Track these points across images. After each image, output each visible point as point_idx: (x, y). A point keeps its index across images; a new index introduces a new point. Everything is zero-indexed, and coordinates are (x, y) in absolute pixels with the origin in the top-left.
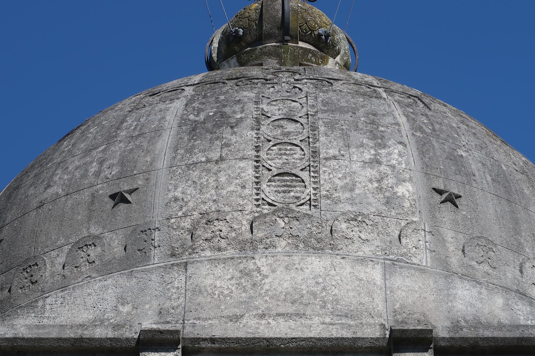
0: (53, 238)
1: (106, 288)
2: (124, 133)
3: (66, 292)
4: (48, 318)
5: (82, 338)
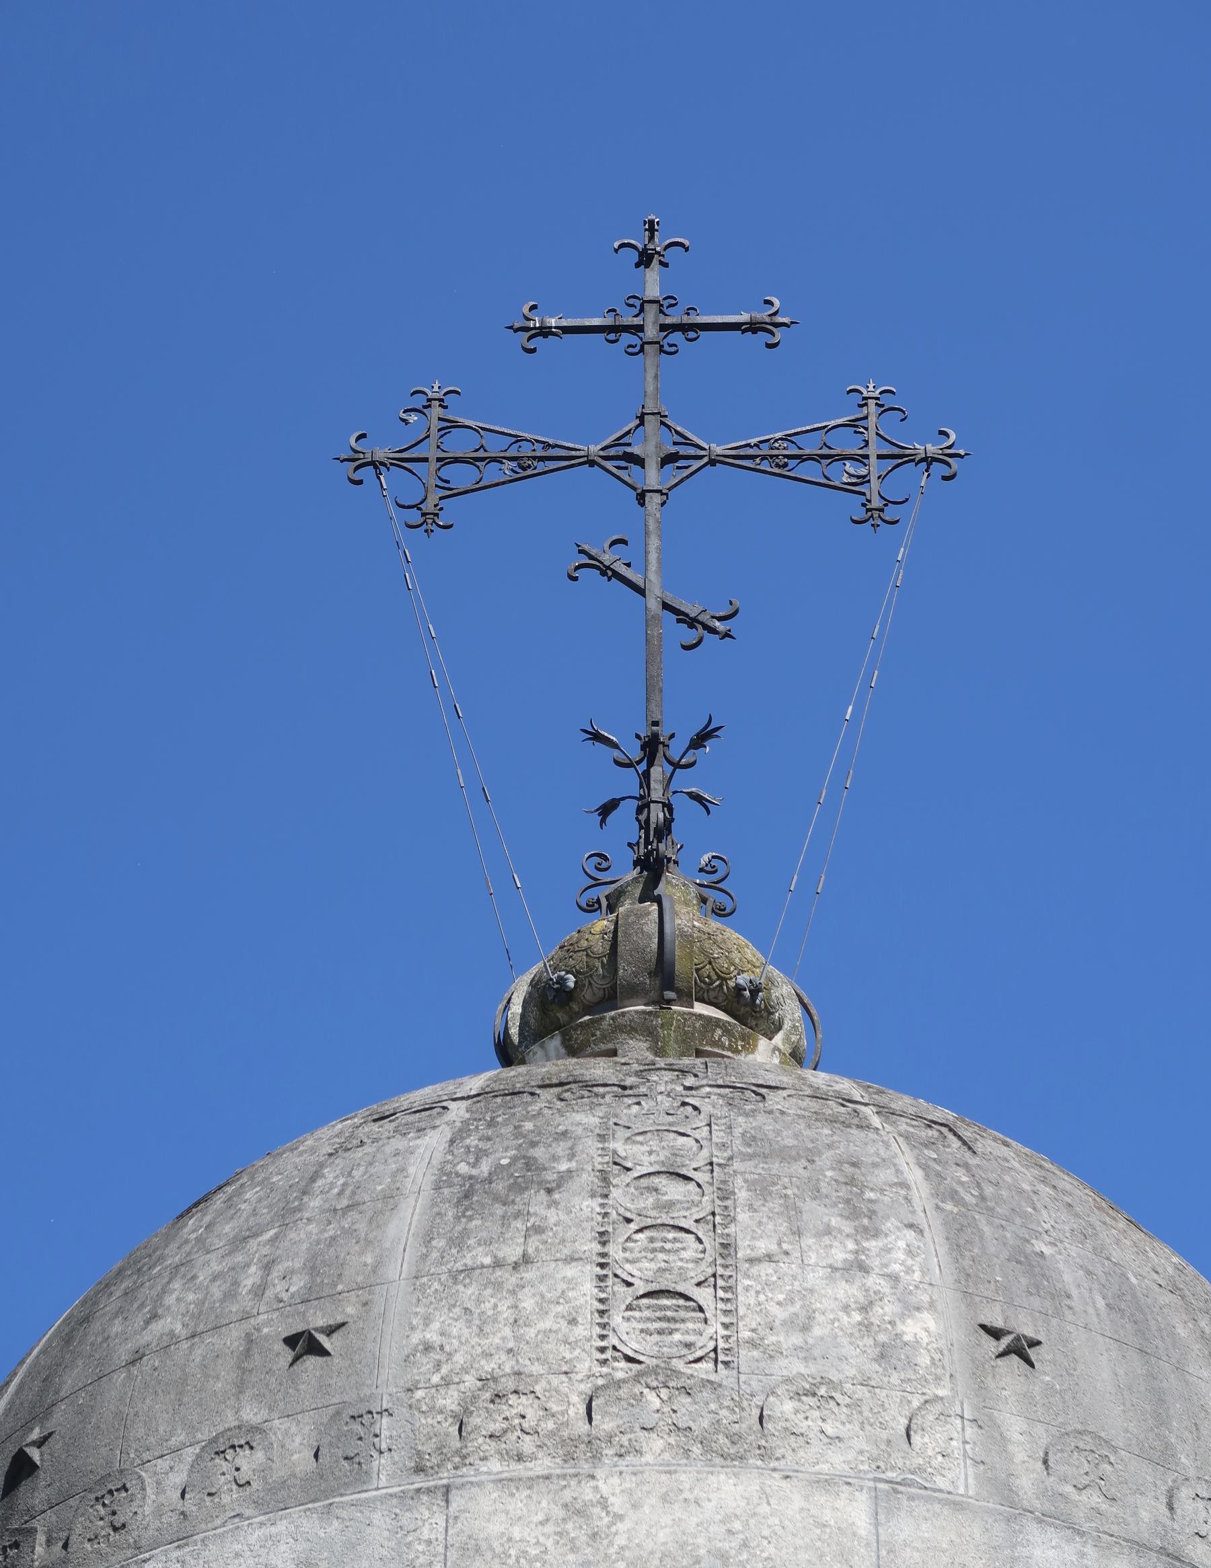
0: (161, 1429)
1: (275, 1540)
3: (187, 1549)
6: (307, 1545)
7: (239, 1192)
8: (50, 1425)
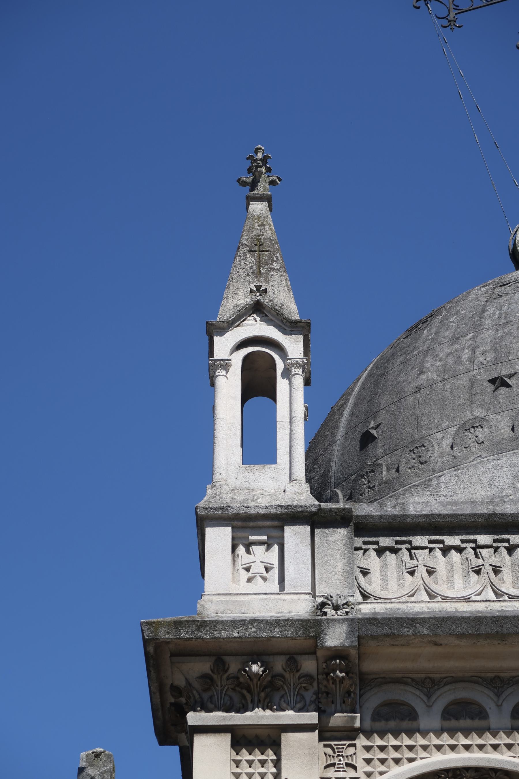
0: (436, 420)
1: (501, 466)
2: (489, 322)
3: (460, 471)
4: (445, 495)
5: (496, 514)
6: (516, 468)
7: (446, 317)
8: (379, 420)
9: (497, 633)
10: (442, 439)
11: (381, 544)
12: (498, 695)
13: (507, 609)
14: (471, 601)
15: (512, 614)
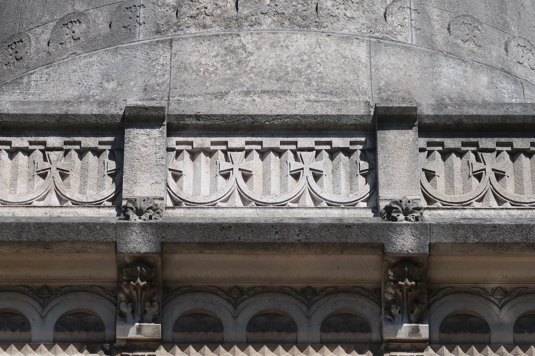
1: (92, 64)
3: (51, 68)
5: (68, 114)
9: (39, 241)
10: (40, 34)
11: (515, 146)
12: (43, 306)
13: (67, 216)
14: (31, 207)
15: (58, 221)
